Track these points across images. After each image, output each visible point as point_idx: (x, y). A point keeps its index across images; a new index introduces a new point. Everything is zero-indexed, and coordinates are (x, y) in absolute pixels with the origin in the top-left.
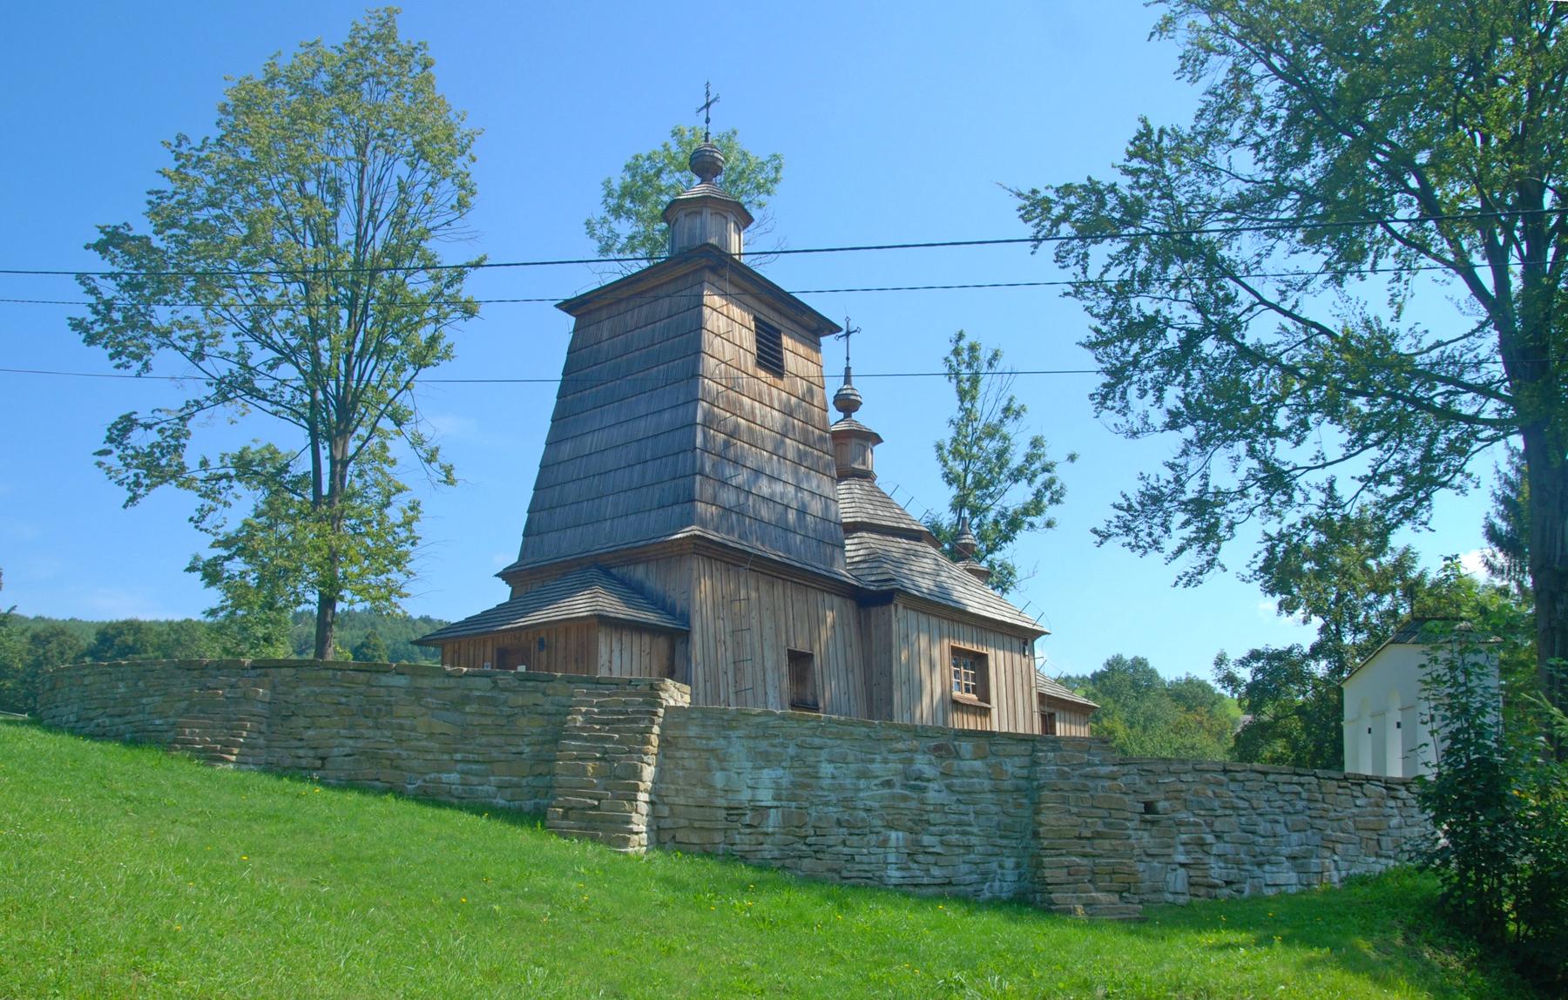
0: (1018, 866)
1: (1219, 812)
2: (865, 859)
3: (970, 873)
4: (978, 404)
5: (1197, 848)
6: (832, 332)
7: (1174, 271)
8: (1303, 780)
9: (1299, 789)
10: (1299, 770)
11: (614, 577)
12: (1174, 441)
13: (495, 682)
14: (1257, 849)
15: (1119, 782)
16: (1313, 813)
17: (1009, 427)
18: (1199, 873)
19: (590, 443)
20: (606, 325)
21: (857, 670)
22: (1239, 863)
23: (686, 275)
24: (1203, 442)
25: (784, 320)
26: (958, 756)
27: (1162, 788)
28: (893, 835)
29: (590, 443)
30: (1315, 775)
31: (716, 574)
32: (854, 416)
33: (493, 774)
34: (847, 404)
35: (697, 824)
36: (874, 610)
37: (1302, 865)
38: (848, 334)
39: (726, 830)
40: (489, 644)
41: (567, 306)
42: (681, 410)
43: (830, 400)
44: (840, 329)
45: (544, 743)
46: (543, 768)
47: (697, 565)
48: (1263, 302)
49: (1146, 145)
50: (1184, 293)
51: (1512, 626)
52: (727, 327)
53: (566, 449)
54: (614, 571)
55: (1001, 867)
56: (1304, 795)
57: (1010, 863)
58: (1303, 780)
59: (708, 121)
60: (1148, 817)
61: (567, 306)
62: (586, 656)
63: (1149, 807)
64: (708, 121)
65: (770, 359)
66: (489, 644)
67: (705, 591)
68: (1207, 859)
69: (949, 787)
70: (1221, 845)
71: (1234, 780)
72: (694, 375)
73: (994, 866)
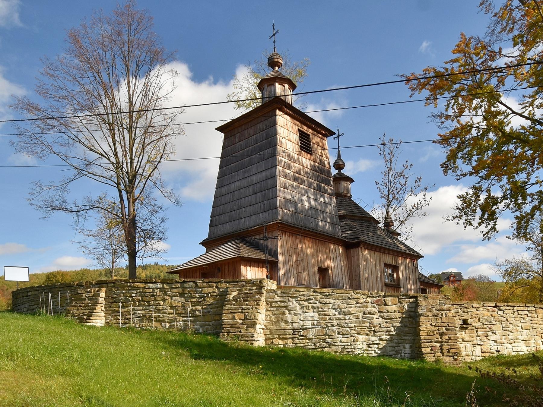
0: (411, 347)
1: (494, 323)
2: (349, 347)
3: (392, 351)
4: (393, 164)
5: (485, 338)
6: (331, 135)
7: (475, 102)
8: (529, 309)
9: (527, 312)
10: (527, 305)
11: (247, 241)
12: (474, 180)
13: (196, 284)
14: (510, 337)
15: (452, 311)
16: (533, 322)
17: (406, 173)
18: (486, 348)
19: (233, 186)
20: (237, 136)
21: (346, 275)
22: (502, 344)
23: (269, 112)
24: (487, 177)
25: (311, 131)
26: (386, 304)
27: (470, 313)
28: (360, 337)
29: (233, 186)
30: (534, 307)
31: (288, 238)
32: (342, 171)
33: (198, 321)
34: (339, 166)
35: (281, 337)
36: (352, 250)
37: (528, 343)
38: (338, 136)
39: (293, 339)
40: (198, 271)
41: (220, 129)
42: (270, 170)
43: (332, 165)
44: (335, 134)
45: (217, 308)
46: (217, 318)
47: (279, 235)
48: (513, 112)
49: (463, 48)
50: (480, 112)
51: (533, 287)
52: (286, 130)
53: (224, 189)
54: (247, 239)
55: (404, 348)
56: (529, 315)
57: (407, 346)
58: (529, 309)
59: (274, 42)
60: (465, 326)
61: (220, 129)
62: (236, 273)
63: (465, 322)
64: (274, 42)
65: (306, 146)
66: (198, 271)
67: (282, 244)
68: (488, 342)
69: (381, 316)
70: (495, 336)
71: (500, 310)
72: (274, 154)
73: (402, 347)
